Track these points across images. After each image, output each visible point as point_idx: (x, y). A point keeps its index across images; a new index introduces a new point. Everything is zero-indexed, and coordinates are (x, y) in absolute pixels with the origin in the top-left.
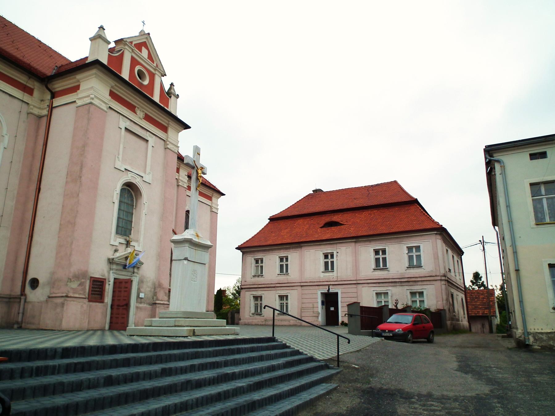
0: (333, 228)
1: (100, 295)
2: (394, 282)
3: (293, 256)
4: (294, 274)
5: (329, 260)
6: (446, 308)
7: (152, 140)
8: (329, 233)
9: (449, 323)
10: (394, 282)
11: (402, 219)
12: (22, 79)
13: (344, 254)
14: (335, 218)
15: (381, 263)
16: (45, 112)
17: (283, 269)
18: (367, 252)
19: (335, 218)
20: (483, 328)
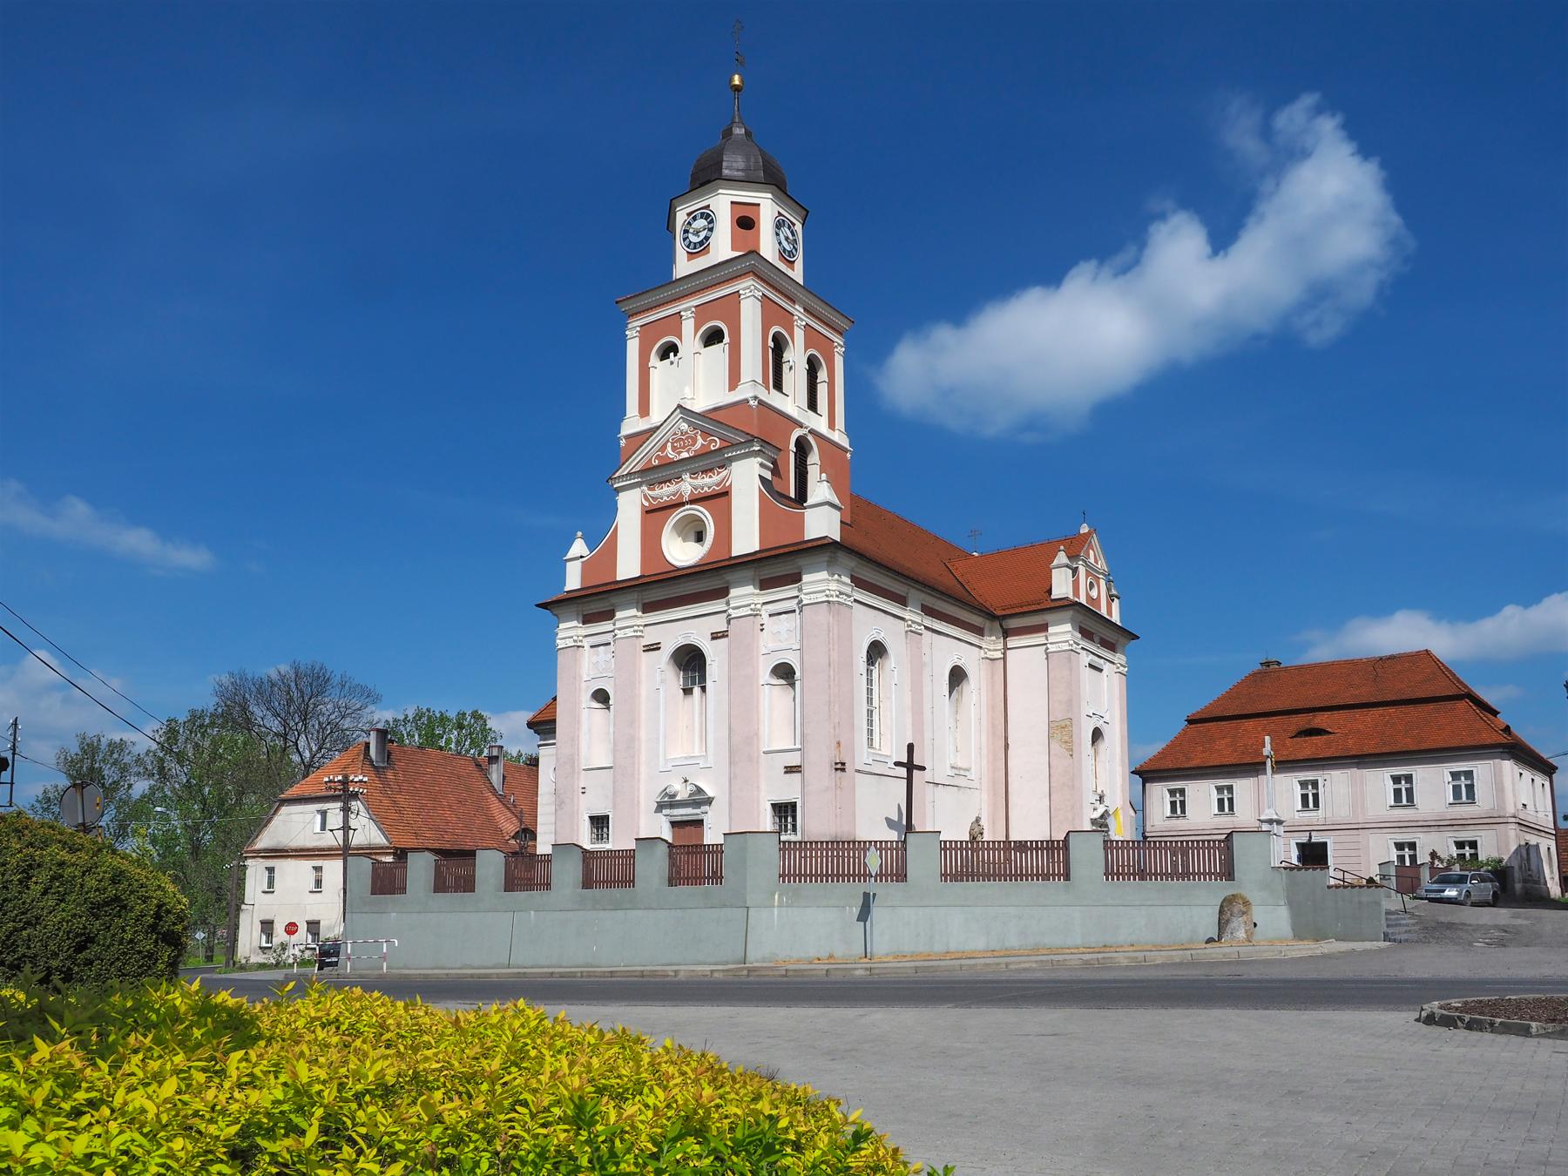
0: (1315, 739)
1: (1185, 853)
2: (1427, 826)
3: (1243, 788)
4: (1245, 815)
5: (1310, 791)
6: (1515, 864)
7: (1107, 667)
8: (1308, 747)
9: (1518, 886)
10: (1427, 826)
11: (1456, 722)
12: (977, 620)
13: (1337, 784)
14: (1320, 720)
15: (1404, 794)
16: (999, 655)
17: (1226, 804)
18: (1379, 781)
19: (1320, 720)
20: (1070, 701)
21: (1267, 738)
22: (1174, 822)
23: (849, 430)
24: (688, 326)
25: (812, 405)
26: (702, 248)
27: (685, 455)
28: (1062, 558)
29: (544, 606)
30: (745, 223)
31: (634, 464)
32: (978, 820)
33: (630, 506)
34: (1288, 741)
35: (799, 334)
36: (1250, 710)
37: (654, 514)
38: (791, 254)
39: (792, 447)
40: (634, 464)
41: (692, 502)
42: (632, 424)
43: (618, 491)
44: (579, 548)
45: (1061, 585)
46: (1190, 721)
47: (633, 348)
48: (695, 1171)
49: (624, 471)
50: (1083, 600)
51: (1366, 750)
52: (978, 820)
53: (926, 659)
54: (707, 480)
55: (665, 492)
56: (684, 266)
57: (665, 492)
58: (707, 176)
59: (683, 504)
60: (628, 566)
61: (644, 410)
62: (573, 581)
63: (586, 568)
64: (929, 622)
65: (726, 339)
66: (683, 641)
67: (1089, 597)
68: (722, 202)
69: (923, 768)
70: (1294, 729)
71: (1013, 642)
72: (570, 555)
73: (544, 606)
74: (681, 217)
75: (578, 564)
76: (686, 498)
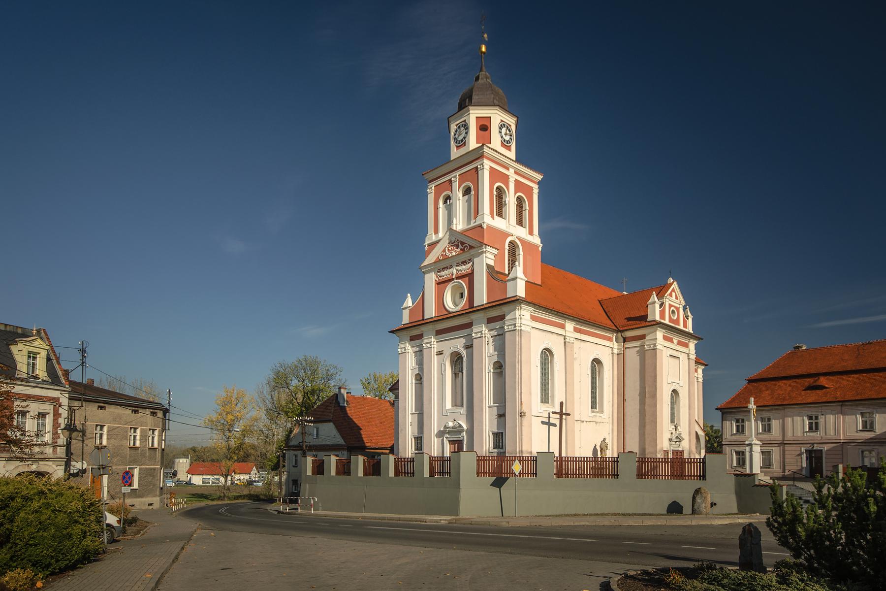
8: (813, 396)
14: (823, 381)
19: (823, 381)
21: (752, 399)
22: (738, 437)
23: (541, 234)
24: (456, 185)
25: (520, 222)
26: (462, 143)
27: (454, 254)
28: (654, 297)
29: (393, 332)
30: (484, 127)
31: (430, 259)
32: (604, 439)
33: (430, 279)
34: (803, 393)
35: (512, 186)
36: (783, 374)
37: (441, 284)
38: (508, 142)
39: (507, 247)
40: (430, 259)
41: (457, 278)
42: (431, 237)
43: (424, 273)
44: (409, 302)
45: (655, 313)
46: (750, 381)
47: (431, 198)
48: (2, 421)
49: (426, 263)
50: (667, 322)
51: (847, 398)
52: (604, 439)
53: (575, 356)
54: (464, 267)
55: (445, 274)
56: (455, 153)
57: (445, 274)
58: (465, 103)
59: (453, 279)
60: (431, 311)
61: (436, 231)
62: (406, 319)
63: (412, 311)
64: (578, 335)
65: (473, 192)
66: (453, 350)
67: (671, 320)
68: (474, 114)
69: (569, 415)
70: (806, 385)
71: (628, 345)
72: (405, 305)
73: (393, 332)
74: (453, 127)
75: (407, 311)
76: (454, 276)
